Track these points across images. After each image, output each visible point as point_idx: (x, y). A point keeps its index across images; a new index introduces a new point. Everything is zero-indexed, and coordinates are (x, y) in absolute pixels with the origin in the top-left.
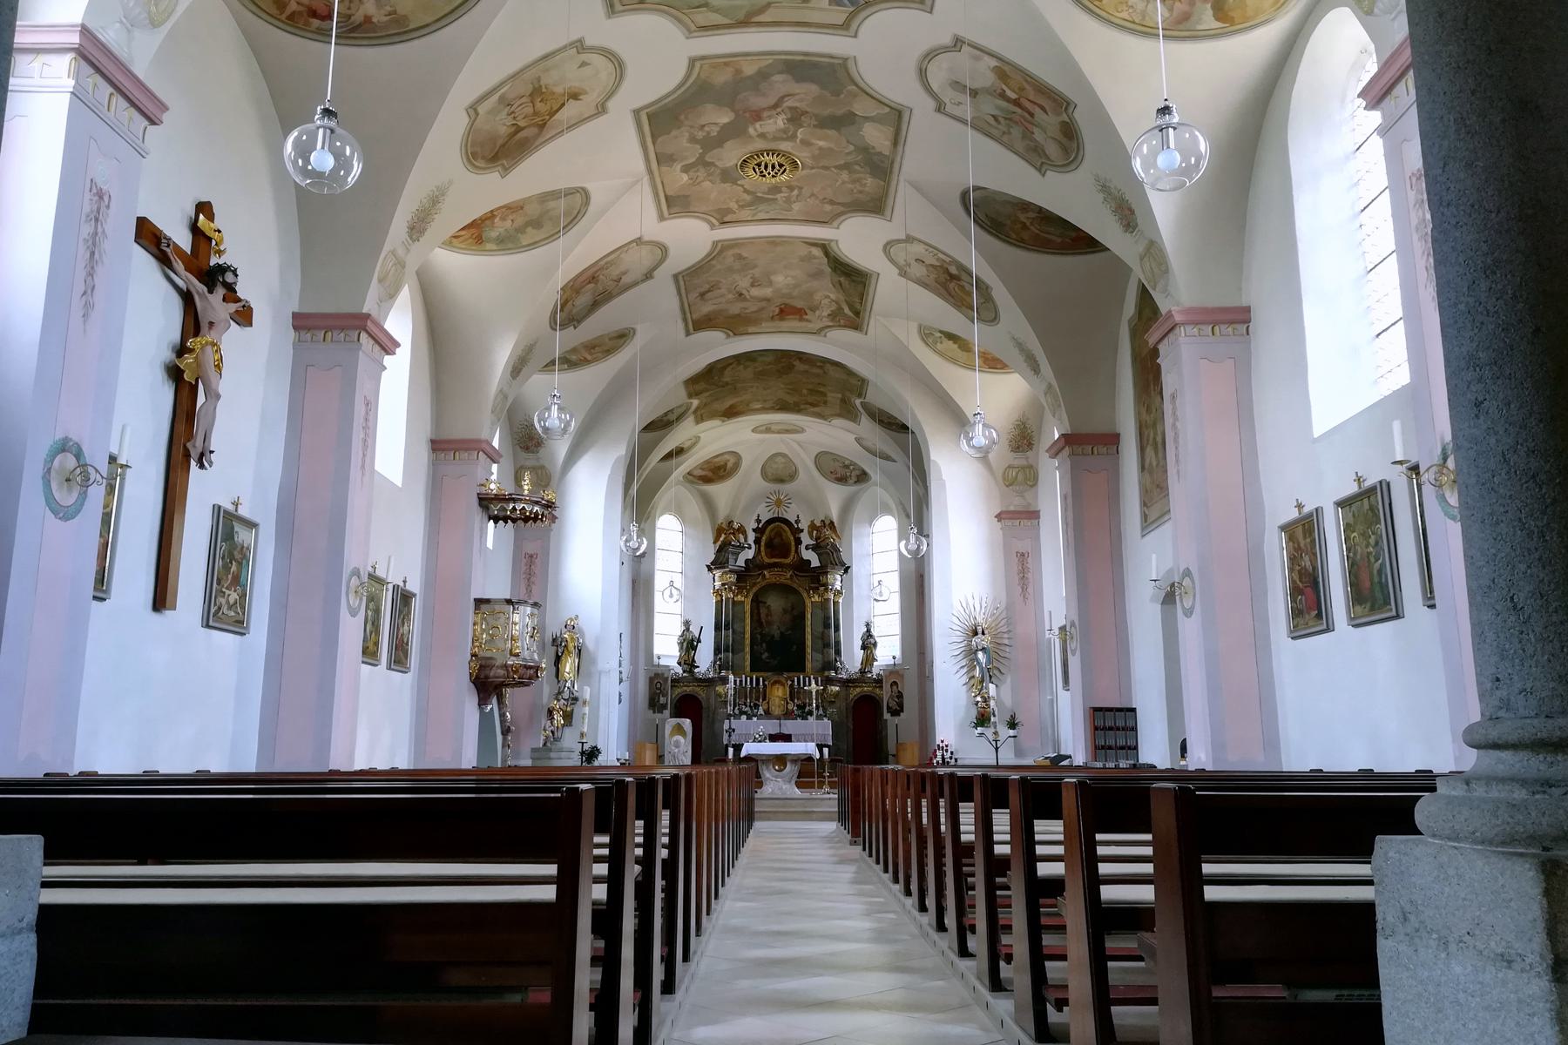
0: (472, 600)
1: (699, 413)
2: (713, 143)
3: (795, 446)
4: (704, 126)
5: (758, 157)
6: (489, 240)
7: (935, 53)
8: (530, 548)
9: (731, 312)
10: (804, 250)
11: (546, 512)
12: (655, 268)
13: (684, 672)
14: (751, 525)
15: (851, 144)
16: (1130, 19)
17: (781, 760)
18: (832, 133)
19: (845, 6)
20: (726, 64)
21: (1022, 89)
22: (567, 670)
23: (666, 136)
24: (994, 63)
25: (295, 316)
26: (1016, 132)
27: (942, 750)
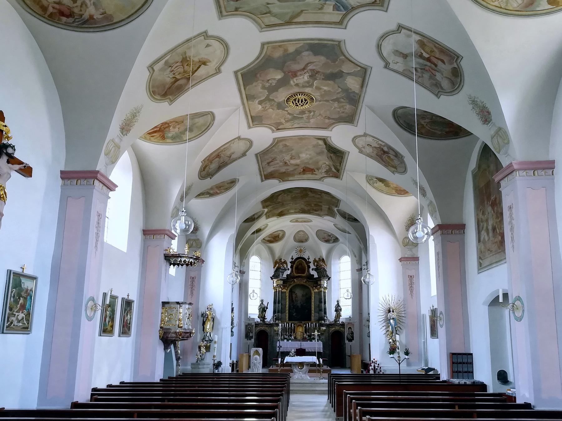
0: (161, 302)
1: (268, 214)
2: (273, 89)
3: (308, 228)
4: (269, 80)
5: (295, 96)
6: (168, 138)
7: (387, 35)
8: (192, 274)
9: (281, 171)
10: (315, 142)
11: (196, 262)
12: (247, 151)
13: (261, 321)
14: (289, 261)
15: (340, 88)
16: (499, 6)
17: (301, 364)
18: (330, 82)
19: (341, 11)
20: (280, 46)
21: (432, 51)
22: (208, 328)
23: (250, 86)
24: (418, 38)
25: (62, 172)
26: (426, 76)
27: (374, 363)
